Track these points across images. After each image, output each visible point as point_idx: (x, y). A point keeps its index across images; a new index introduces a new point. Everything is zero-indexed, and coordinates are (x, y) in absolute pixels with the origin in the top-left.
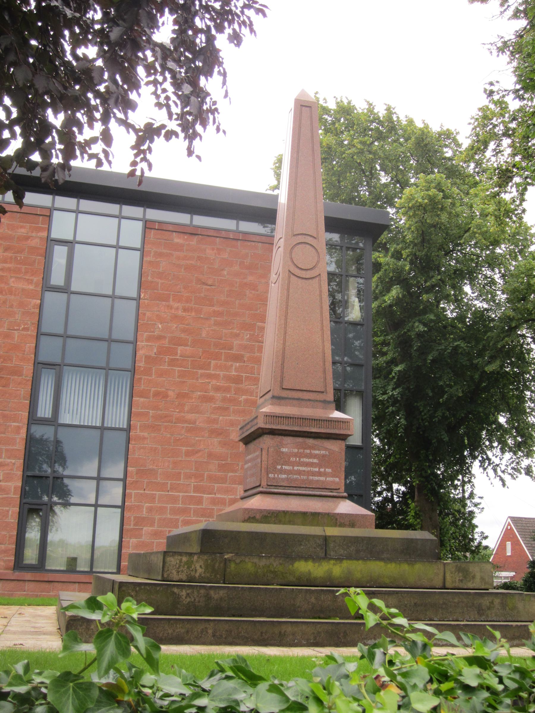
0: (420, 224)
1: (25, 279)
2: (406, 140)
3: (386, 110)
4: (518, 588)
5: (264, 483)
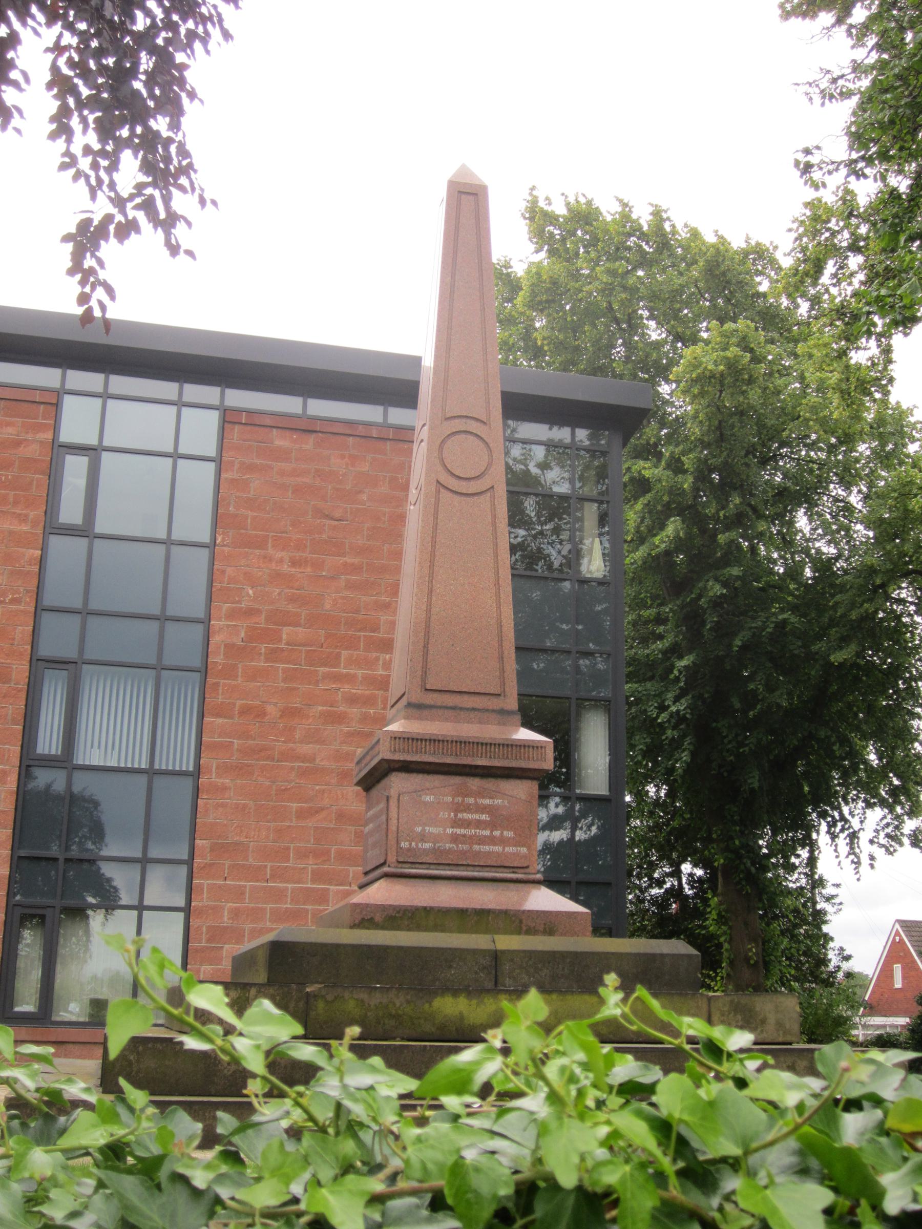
0: (714, 409)
1: (14, 513)
2: (689, 265)
3: (652, 214)
4: (901, 1044)
5: (392, 859)
